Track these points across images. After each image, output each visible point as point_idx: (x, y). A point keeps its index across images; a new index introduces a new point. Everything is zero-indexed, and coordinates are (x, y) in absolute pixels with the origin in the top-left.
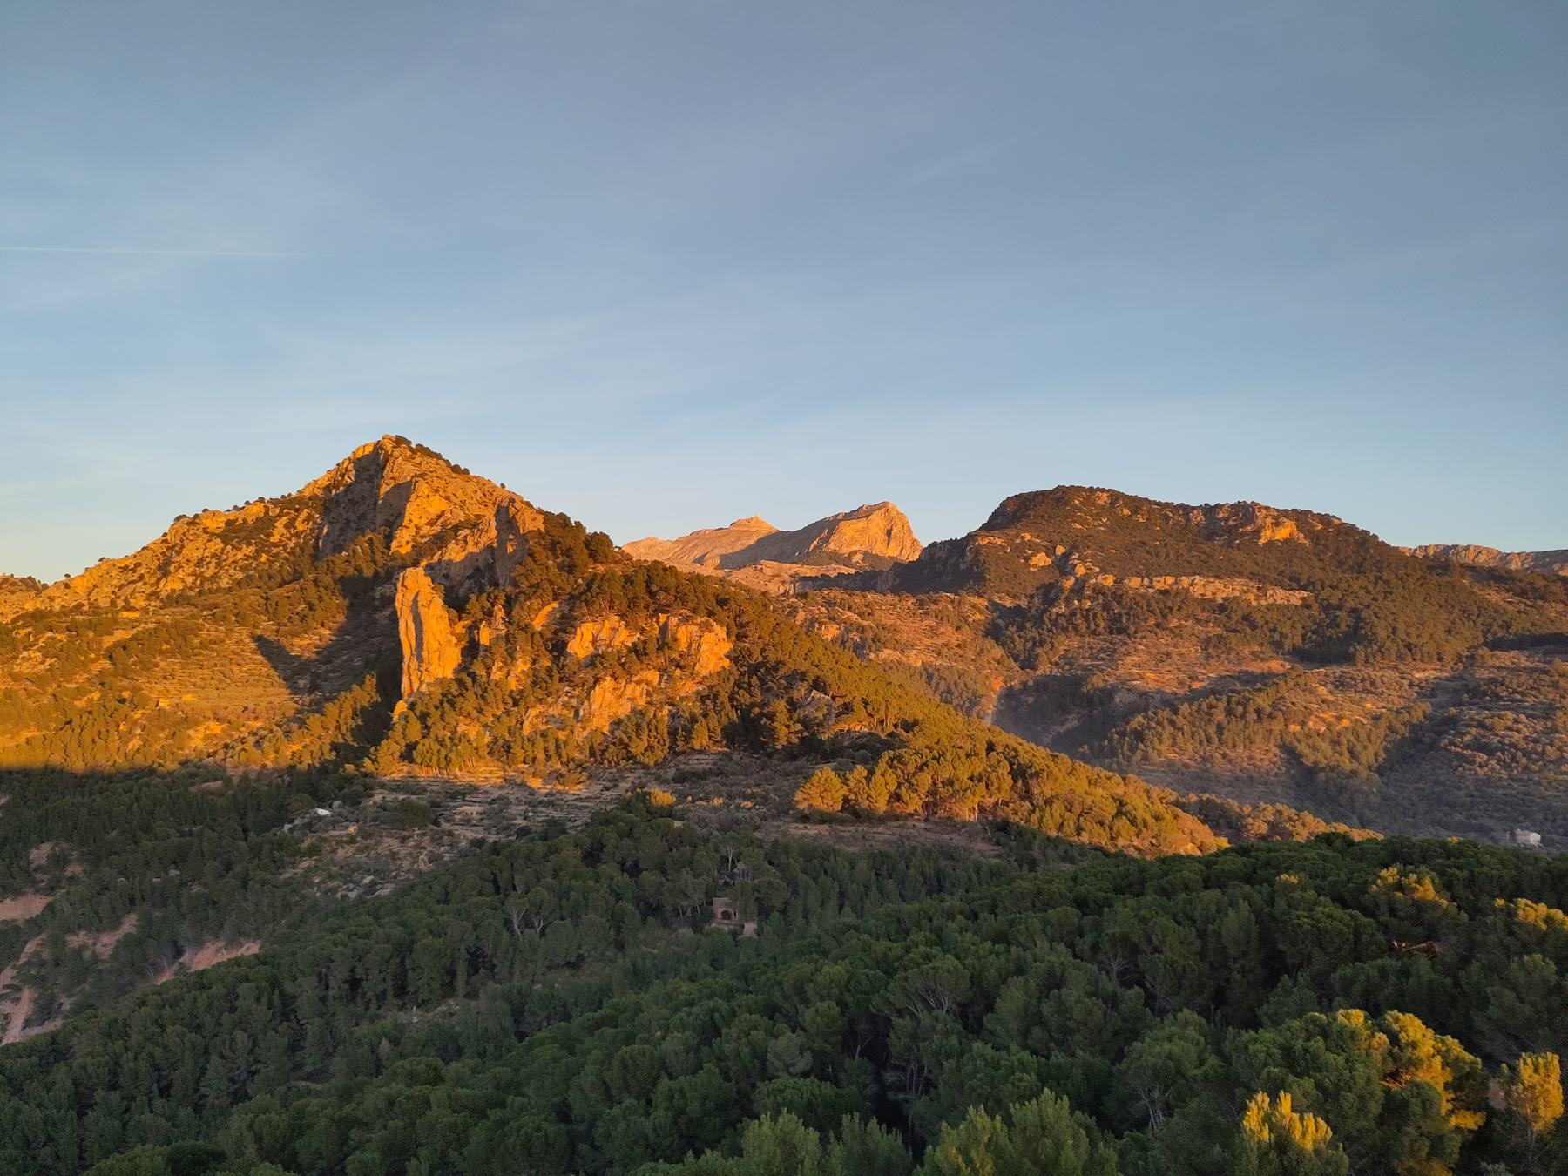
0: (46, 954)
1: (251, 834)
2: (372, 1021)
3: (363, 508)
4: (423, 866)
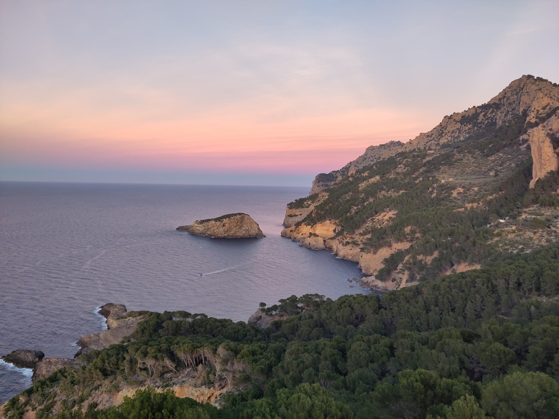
0: (411, 261)
1: (476, 227)
2: (527, 299)
3: (514, 106)
4: (544, 243)
